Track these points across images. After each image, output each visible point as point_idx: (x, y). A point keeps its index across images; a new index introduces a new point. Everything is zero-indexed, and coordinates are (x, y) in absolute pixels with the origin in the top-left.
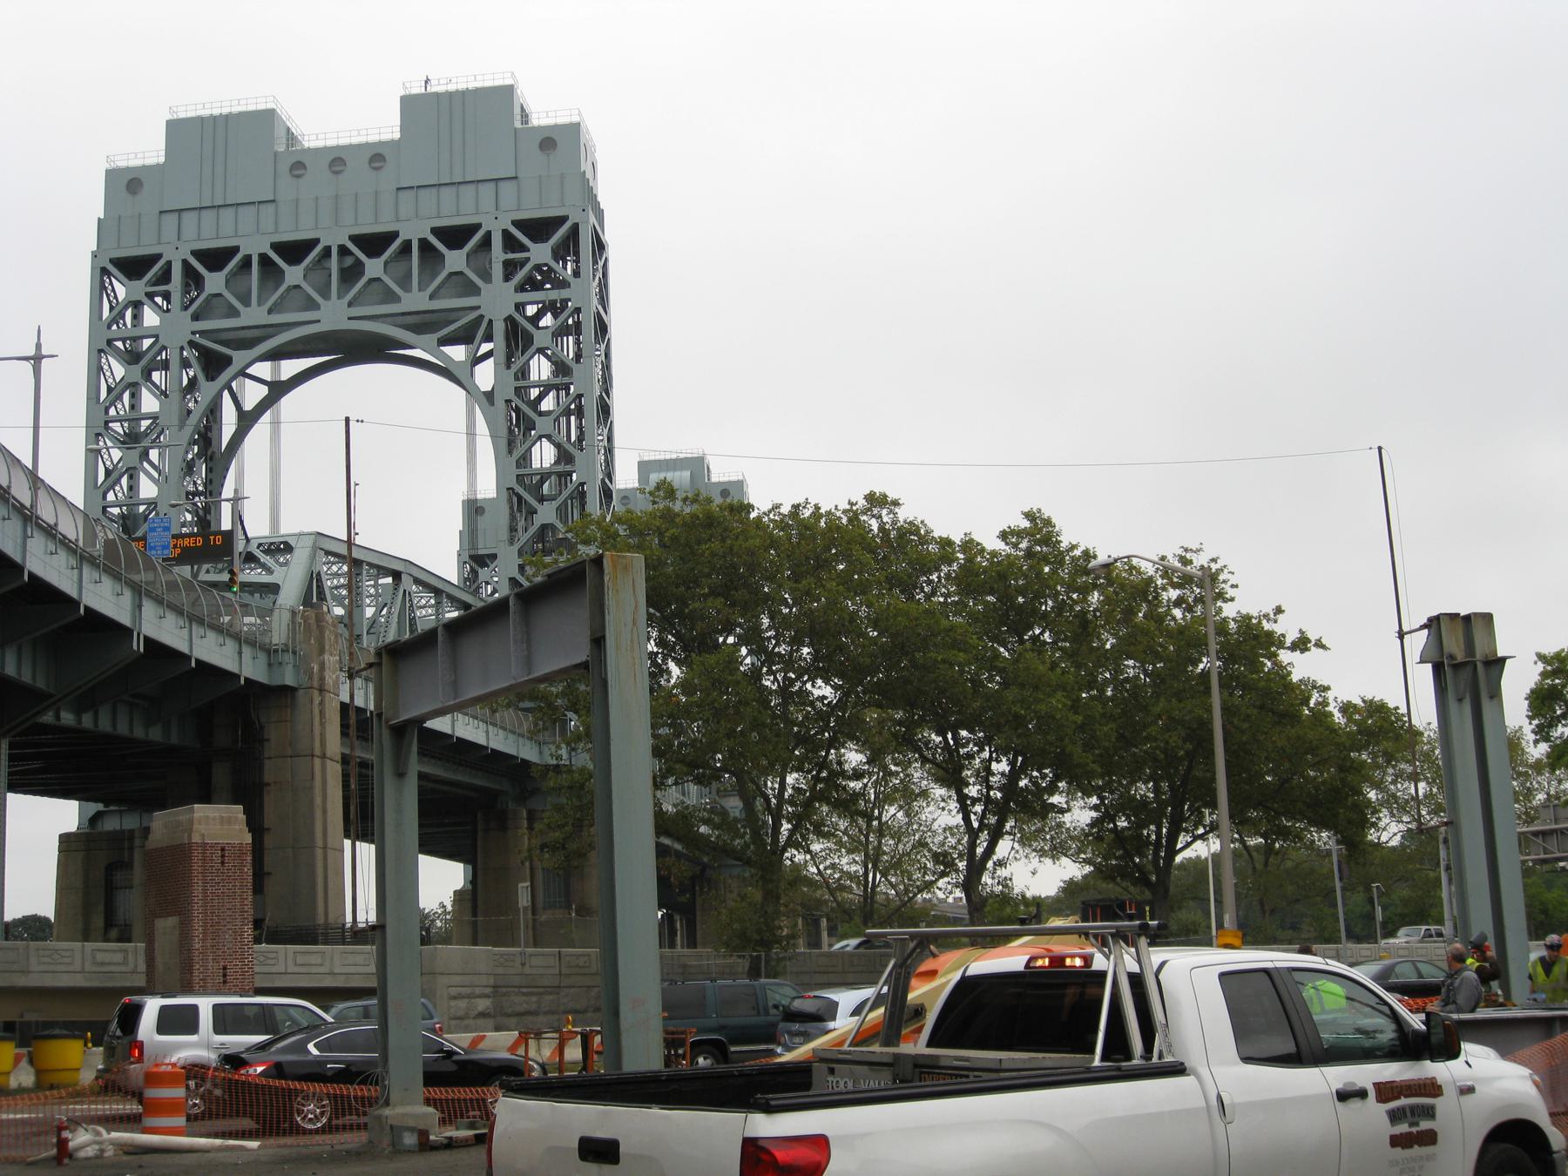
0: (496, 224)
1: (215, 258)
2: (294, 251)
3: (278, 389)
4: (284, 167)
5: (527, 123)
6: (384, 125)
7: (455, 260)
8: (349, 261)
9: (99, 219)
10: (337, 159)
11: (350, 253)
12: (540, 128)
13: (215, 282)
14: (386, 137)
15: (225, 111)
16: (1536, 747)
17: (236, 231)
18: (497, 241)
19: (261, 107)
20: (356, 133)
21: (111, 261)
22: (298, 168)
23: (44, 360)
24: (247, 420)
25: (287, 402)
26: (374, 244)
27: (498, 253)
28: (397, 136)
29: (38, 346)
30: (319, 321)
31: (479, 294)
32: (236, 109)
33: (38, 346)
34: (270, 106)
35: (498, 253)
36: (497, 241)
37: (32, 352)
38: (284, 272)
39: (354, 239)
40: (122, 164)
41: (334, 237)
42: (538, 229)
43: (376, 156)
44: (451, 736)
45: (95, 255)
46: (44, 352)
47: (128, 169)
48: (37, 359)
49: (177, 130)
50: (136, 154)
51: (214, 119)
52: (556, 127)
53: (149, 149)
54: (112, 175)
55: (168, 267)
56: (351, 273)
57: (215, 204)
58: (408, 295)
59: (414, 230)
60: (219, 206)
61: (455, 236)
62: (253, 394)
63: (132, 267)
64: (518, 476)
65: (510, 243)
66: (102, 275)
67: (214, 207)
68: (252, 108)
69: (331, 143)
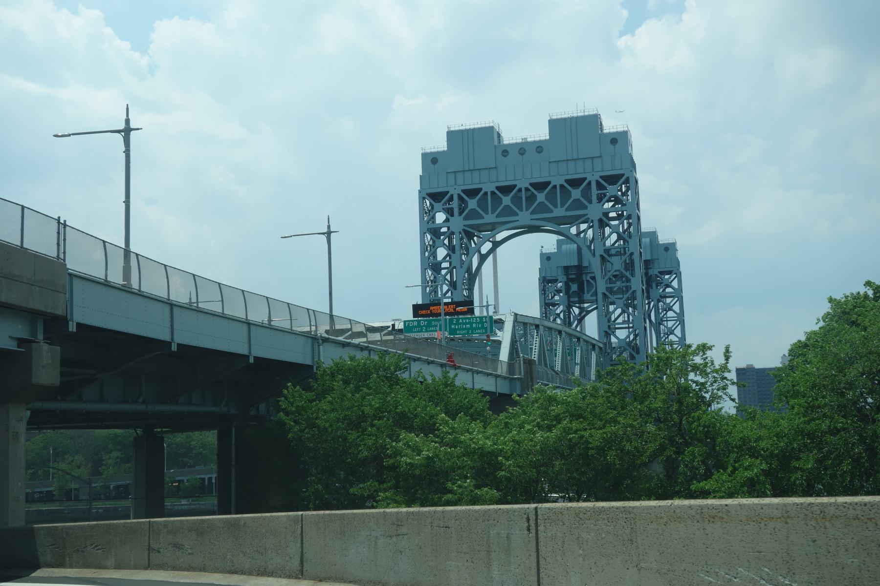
0: (594, 178)
1: (472, 193)
2: (506, 190)
3: (496, 245)
4: (499, 152)
5: (500, 143)
6: (541, 133)
7: (576, 193)
8: (529, 194)
9: (420, 176)
10: (522, 148)
11: (530, 190)
12: (610, 133)
13: (472, 204)
14: (543, 138)
15: (472, 127)
16: (734, 407)
17: (549, 173)
18: (594, 185)
19: (487, 125)
20: (529, 137)
21: (427, 194)
22: (505, 153)
23: (332, 234)
24: (483, 258)
25: (499, 250)
26: (541, 186)
27: (594, 191)
28: (446, 149)
29: (329, 227)
30: (518, 221)
31: (587, 209)
32: (477, 126)
33: (329, 227)
34: (491, 125)
35: (594, 191)
36: (594, 185)
37: (325, 230)
38: (571, 192)
39: (531, 184)
40: (429, 151)
41: (523, 184)
42: (613, 179)
43: (539, 147)
44: (168, 344)
45: (420, 192)
46: (332, 230)
47: (431, 153)
48: (328, 234)
49: (452, 135)
50: (531, 136)
51: (468, 131)
52: (617, 133)
53: (440, 144)
54: (425, 156)
55: (452, 197)
56: (531, 199)
57: (574, 158)
58: (522, 212)
59: (558, 181)
60: (576, 159)
61: (575, 183)
62: (487, 246)
63: (436, 197)
64: (606, 287)
65: (599, 186)
66: (422, 199)
67: (469, 170)
68: (483, 126)
69: (537, 139)
